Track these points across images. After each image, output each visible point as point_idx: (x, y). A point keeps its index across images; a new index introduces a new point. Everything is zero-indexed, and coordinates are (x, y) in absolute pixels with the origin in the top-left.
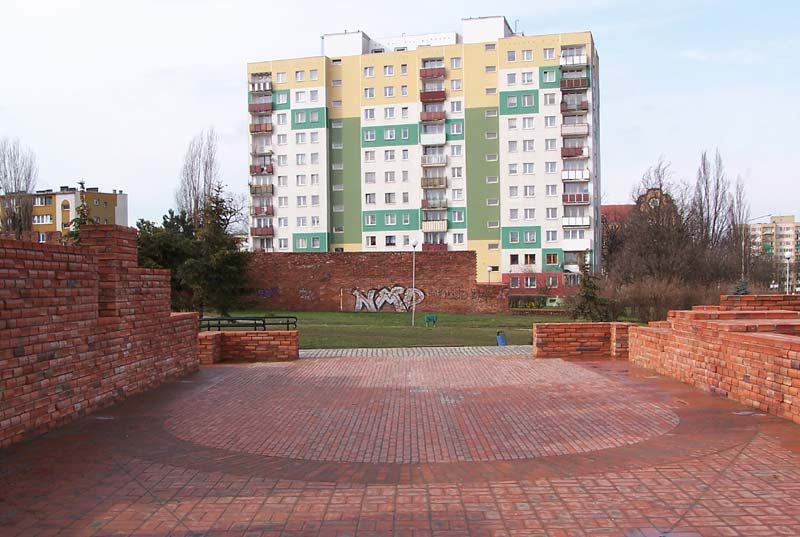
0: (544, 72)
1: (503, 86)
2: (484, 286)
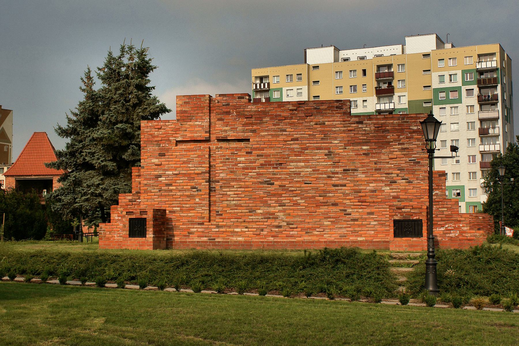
0: (464, 72)
1: (436, 84)
2: (513, 235)
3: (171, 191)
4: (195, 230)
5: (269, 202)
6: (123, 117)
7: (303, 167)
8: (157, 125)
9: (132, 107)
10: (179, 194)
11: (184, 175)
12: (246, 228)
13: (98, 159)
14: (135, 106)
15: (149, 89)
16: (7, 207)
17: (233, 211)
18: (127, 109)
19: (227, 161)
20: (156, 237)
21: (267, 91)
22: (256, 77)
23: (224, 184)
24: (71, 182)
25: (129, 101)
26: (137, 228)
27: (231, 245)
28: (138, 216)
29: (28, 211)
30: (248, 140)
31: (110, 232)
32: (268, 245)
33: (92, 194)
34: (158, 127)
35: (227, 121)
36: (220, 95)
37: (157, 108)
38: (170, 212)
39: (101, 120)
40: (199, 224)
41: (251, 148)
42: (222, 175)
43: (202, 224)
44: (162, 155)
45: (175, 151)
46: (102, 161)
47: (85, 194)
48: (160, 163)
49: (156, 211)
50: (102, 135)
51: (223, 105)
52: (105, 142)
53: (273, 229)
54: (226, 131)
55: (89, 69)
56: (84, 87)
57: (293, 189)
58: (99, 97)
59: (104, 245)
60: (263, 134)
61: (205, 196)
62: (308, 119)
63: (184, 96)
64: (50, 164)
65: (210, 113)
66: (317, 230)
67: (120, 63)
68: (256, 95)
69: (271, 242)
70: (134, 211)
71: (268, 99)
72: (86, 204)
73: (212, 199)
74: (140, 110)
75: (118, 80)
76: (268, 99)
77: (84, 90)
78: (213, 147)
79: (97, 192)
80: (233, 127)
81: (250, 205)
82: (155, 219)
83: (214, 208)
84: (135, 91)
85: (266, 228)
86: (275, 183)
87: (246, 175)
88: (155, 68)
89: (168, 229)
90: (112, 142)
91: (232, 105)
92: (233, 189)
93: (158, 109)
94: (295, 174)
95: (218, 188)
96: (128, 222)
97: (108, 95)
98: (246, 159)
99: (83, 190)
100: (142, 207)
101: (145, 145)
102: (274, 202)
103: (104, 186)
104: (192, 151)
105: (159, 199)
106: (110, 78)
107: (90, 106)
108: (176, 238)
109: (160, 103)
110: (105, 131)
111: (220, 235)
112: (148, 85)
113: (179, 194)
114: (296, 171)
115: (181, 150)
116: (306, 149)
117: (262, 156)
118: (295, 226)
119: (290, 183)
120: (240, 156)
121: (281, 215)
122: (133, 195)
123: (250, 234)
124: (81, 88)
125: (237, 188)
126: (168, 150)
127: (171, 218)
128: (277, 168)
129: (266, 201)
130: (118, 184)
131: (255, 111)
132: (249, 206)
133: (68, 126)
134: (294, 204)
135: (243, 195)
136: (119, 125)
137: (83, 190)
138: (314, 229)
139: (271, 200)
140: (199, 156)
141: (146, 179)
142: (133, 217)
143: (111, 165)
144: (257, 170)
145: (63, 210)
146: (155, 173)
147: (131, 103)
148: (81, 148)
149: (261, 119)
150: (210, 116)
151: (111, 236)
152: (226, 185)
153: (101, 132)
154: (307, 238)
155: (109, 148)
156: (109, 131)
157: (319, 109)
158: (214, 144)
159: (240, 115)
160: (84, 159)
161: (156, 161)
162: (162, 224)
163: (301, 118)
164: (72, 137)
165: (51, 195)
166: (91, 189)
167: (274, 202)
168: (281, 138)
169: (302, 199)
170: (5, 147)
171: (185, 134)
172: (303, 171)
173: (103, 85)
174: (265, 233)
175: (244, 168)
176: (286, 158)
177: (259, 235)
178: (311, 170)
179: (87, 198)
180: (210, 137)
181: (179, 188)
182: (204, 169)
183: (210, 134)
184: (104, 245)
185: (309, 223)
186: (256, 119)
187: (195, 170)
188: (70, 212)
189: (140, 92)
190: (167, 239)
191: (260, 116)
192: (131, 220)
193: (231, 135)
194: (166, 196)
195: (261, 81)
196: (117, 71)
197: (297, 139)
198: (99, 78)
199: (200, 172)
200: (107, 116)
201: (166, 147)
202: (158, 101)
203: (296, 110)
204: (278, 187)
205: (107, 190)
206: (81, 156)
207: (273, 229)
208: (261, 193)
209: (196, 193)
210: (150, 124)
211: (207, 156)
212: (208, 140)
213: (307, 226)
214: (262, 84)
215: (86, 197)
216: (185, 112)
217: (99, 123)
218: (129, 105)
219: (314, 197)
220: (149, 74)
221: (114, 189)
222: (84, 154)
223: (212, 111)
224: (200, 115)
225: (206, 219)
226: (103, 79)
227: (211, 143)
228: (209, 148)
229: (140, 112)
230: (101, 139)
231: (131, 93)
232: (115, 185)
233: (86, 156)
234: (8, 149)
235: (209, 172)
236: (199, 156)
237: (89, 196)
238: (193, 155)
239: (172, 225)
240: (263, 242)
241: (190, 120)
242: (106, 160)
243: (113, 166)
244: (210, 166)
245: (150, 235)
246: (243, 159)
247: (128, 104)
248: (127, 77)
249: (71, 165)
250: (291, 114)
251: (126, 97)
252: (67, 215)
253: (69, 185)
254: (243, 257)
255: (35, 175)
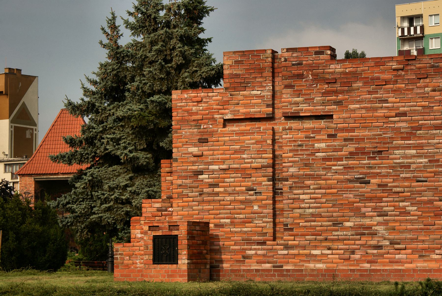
3: (217, 194)
4: (253, 252)
5: (363, 210)
6: (161, 85)
7: (414, 156)
8: (195, 97)
9: (175, 70)
10: (228, 198)
11: (237, 170)
12: (329, 249)
13: (125, 148)
14: (179, 68)
15: (202, 42)
16: (7, 221)
17: (308, 224)
18: (168, 73)
19: (299, 148)
20: (193, 263)
21: (420, 38)
22: (403, 18)
23: (295, 183)
24: (86, 183)
25: (171, 61)
26: (164, 250)
27: (306, 275)
28: (166, 232)
29: (37, 227)
30: (330, 117)
31: (130, 256)
32: (361, 275)
33: (116, 199)
34: (197, 99)
35: (299, 88)
36: (288, 50)
37: (211, 70)
38: (216, 225)
39: (129, 90)
40: (259, 244)
41: (336, 130)
42: (292, 170)
43: (263, 243)
44: (203, 141)
45: (223, 135)
46: (131, 152)
47: (106, 200)
48: (200, 153)
49: (192, 225)
50: (129, 113)
51: (293, 65)
52: (134, 123)
53: (370, 251)
54: (297, 103)
55: (113, 14)
56: (106, 41)
57: (398, 189)
58: (127, 56)
59: (122, 276)
60: (352, 106)
61: (267, 202)
62: (422, 83)
63: (235, 52)
64: (58, 157)
65: (273, 77)
66: (437, 251)
67: (157, 4)
68: (403, 45)
69: (366, 270)
70: (160, 225)
71: (421, 52)
72: (107, 215)
73: (278, 206)
74: (186, 74)
75: (155, 30)
76: (421, 52)
77: (105, 46)
78: (279, 128)
79: (124, 197)
80: (307, 97)
81: (335, 214)
82: (191, 236)
83: (281, 220)
84: (179, 45)
85: (359, 249)
86: (373, 181)
87: (328, 169)
88: (212, 10)
89: (212, 251)
90: (144, 123)
91: (306, 64)
92: (309, 191)
93: (213, 72)
94: (401, 167)
95: (286, 189)
96: (151, 242)
97: (141, 53)
98: (328, 146)
99: (103, 194)
100: (175, 218)
101: (178, 127)
102: (370, 209)
103: (134, 188)
104: (248, 134)
105: (200, 207)
106: (143, 27)
107: (113, 70)
108: (225, 265)
109: (216, 63)
110: (135, 107)
111: (290, 260)
112: (201, 36)
113: (228, 198)
114: (403, 163)
115: (232, 133)
116: (419, 128)
117: (352, 140)
118: (404, 246)
119: (394, 181)
120: (319, 141)
121: (381, 229)
122: (163, 201)
123: (336, 258)
124: (101, 43)
125: (314, 189)
126: (212, 134)
127: (217, 235)
128: (374, 158)
129: (358, 209)
130: (155, 186)
131: (341, 73)
132: (332, 216)
133: (82, 100)
134: (401, 213)
135: (324, 200)
136: (156, 98)
137: (103, 194)
138: (432, 250)
139: (365, 207)
140: (257, 142)
141: (180, 177)
142: (159, 233)
143: (144, 157)
144: (344, 162)
145: (76, 225)
146: (194, 168)
147: (173, 63)
148: (101, 132)
149: (349, 84)
150: (273, 82)
151: (131, 262)
152: (298, 185)
153: (131, 107)
154: (421, 265)
155: (141, 131)
156: (142, 106)
157: (438, 66)
158: (280, 124)
159: (318, 79)
160: (106, 149)
161: (194, 150)
162: (202, 244)
163: (411, 82)
164: (90, 117)
165: (59, 203)
166: (115, 192)
167: (370, 209)
168: (380, 113)
169: (412, 205)
170: (28, 133)
171: (237, 109)
172: (414, 163)
173: (132, 38)
174: (357, 256)
175: (325, 159)
176: (388, 143)
177: (349, 259)
178: (426, 160)
179: (109, 207)
180: (273, 113)
181: (229, 189)
182: (265, 162)
183: (274, 108)
184: (122, 276)
185: (423, 241)
186: (343, 84)
187: (252, 162)
188: (86, 227)
189: (186, 48)
190: (212, 267)
191: (347, 81)
192: (155, 238)
193: (305, 109)
194: (209, 202)
195: (411, 24)
196: (152, 17)
197: (404, 114)
198: (126, 27)
199: (259, 165)
200: (137, 83)
201: (209, 130)
202: (214, 61)
203: (402, 70)
204: (376, 187)
205: (138, 194)
206: (102, 145)
207: (370, 251)
208: (351, 196)
209: (254, 197)
210: (186, 96)
211: (270, 142)
212: (270, 118)
213: (420, 246)
214: (412, 29)
215: (107, 205)
216: (237, 76)
217: (127, 94)
218: (171, 67)
219: (431, 202)
220: (204, 20)
221: (147, 192)
222: (105, 141)
223: (276, 75)
224: (259, 80)
225: (269, 236)
226: (132, 29)
227: (276, 121)
228: (273, 129)
229: (186, 78)
230: (129, 118)
231: (174, 48)
232: (151, 186)
233: (108, 143)
234: (32, 135)
235: (273, 166)
236: (257, 142)
237: (112, 203)
238: (248, 140)
239: (219, 245)
240: (353, 271)
241: (245, 88)
242: (136, 150)
243: (146, 158)
244: (274, 157)
245: (183, 260)
246: (323, 145)
247: (170, 65)
248: (168, 24)
249: (88, 158)
250: (396, 76)
251: (166, 55)
252: (82, 232)
253: (84, 188)
254: (305, 292)
255: (63, 174)
